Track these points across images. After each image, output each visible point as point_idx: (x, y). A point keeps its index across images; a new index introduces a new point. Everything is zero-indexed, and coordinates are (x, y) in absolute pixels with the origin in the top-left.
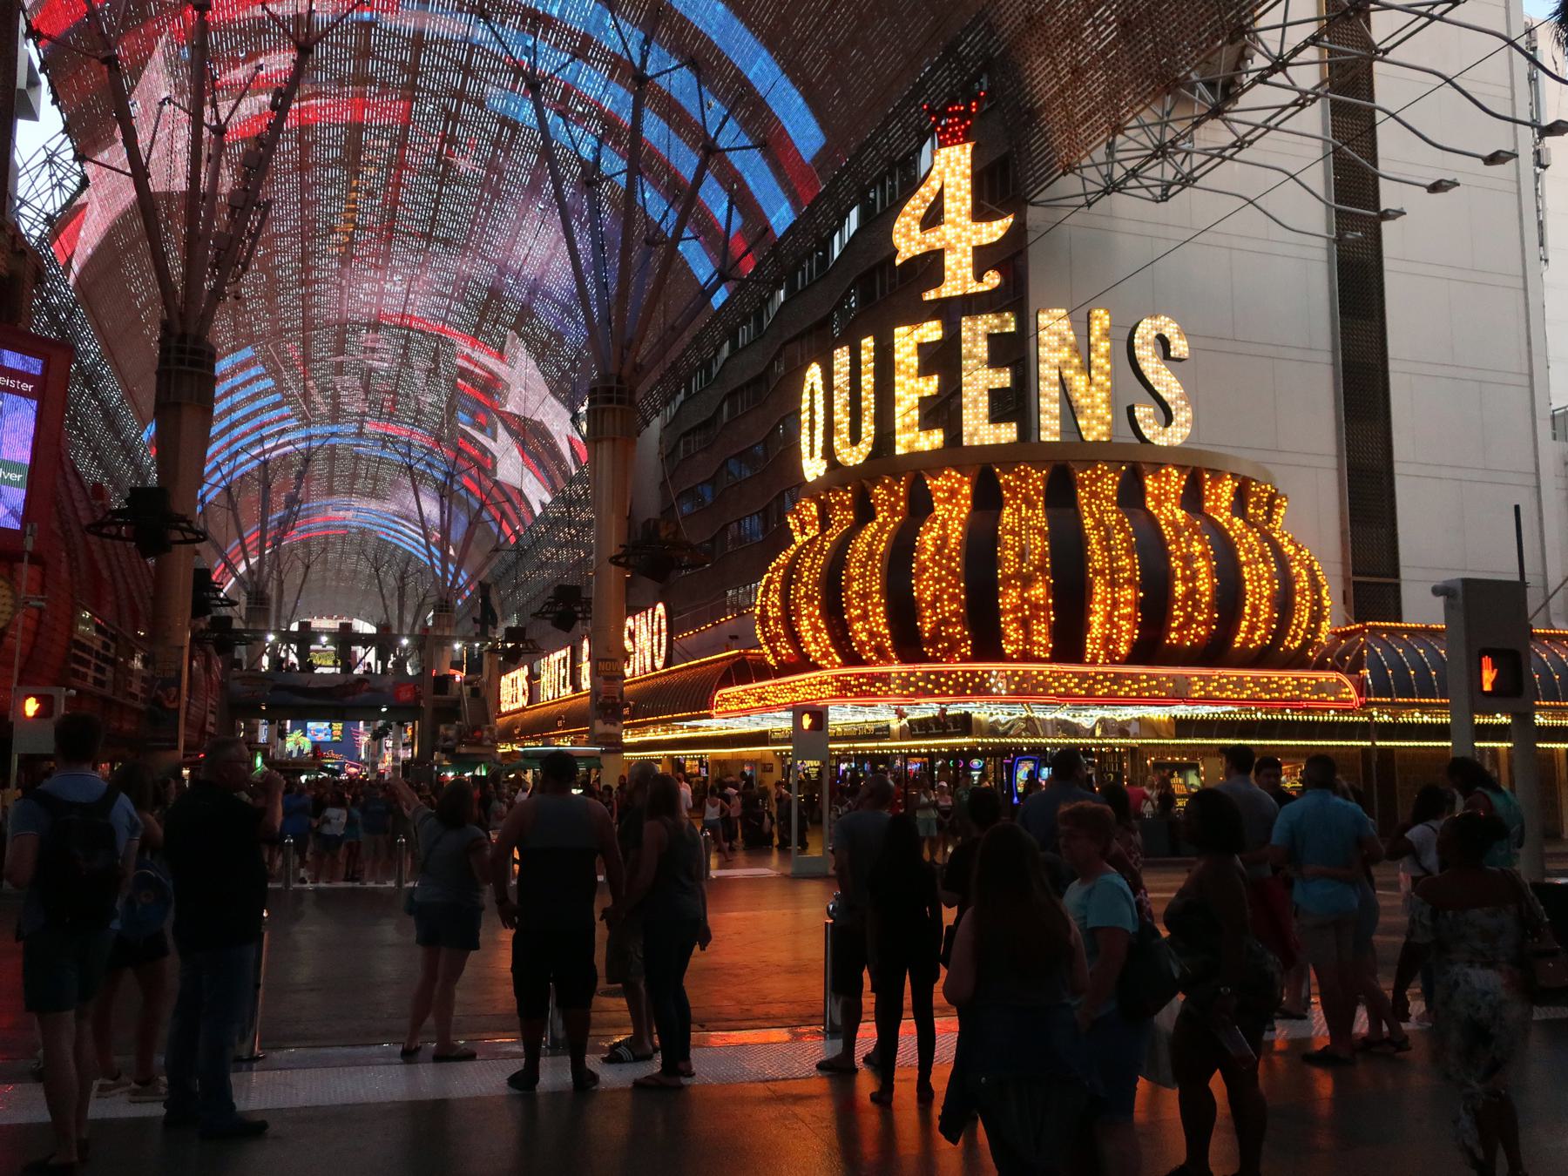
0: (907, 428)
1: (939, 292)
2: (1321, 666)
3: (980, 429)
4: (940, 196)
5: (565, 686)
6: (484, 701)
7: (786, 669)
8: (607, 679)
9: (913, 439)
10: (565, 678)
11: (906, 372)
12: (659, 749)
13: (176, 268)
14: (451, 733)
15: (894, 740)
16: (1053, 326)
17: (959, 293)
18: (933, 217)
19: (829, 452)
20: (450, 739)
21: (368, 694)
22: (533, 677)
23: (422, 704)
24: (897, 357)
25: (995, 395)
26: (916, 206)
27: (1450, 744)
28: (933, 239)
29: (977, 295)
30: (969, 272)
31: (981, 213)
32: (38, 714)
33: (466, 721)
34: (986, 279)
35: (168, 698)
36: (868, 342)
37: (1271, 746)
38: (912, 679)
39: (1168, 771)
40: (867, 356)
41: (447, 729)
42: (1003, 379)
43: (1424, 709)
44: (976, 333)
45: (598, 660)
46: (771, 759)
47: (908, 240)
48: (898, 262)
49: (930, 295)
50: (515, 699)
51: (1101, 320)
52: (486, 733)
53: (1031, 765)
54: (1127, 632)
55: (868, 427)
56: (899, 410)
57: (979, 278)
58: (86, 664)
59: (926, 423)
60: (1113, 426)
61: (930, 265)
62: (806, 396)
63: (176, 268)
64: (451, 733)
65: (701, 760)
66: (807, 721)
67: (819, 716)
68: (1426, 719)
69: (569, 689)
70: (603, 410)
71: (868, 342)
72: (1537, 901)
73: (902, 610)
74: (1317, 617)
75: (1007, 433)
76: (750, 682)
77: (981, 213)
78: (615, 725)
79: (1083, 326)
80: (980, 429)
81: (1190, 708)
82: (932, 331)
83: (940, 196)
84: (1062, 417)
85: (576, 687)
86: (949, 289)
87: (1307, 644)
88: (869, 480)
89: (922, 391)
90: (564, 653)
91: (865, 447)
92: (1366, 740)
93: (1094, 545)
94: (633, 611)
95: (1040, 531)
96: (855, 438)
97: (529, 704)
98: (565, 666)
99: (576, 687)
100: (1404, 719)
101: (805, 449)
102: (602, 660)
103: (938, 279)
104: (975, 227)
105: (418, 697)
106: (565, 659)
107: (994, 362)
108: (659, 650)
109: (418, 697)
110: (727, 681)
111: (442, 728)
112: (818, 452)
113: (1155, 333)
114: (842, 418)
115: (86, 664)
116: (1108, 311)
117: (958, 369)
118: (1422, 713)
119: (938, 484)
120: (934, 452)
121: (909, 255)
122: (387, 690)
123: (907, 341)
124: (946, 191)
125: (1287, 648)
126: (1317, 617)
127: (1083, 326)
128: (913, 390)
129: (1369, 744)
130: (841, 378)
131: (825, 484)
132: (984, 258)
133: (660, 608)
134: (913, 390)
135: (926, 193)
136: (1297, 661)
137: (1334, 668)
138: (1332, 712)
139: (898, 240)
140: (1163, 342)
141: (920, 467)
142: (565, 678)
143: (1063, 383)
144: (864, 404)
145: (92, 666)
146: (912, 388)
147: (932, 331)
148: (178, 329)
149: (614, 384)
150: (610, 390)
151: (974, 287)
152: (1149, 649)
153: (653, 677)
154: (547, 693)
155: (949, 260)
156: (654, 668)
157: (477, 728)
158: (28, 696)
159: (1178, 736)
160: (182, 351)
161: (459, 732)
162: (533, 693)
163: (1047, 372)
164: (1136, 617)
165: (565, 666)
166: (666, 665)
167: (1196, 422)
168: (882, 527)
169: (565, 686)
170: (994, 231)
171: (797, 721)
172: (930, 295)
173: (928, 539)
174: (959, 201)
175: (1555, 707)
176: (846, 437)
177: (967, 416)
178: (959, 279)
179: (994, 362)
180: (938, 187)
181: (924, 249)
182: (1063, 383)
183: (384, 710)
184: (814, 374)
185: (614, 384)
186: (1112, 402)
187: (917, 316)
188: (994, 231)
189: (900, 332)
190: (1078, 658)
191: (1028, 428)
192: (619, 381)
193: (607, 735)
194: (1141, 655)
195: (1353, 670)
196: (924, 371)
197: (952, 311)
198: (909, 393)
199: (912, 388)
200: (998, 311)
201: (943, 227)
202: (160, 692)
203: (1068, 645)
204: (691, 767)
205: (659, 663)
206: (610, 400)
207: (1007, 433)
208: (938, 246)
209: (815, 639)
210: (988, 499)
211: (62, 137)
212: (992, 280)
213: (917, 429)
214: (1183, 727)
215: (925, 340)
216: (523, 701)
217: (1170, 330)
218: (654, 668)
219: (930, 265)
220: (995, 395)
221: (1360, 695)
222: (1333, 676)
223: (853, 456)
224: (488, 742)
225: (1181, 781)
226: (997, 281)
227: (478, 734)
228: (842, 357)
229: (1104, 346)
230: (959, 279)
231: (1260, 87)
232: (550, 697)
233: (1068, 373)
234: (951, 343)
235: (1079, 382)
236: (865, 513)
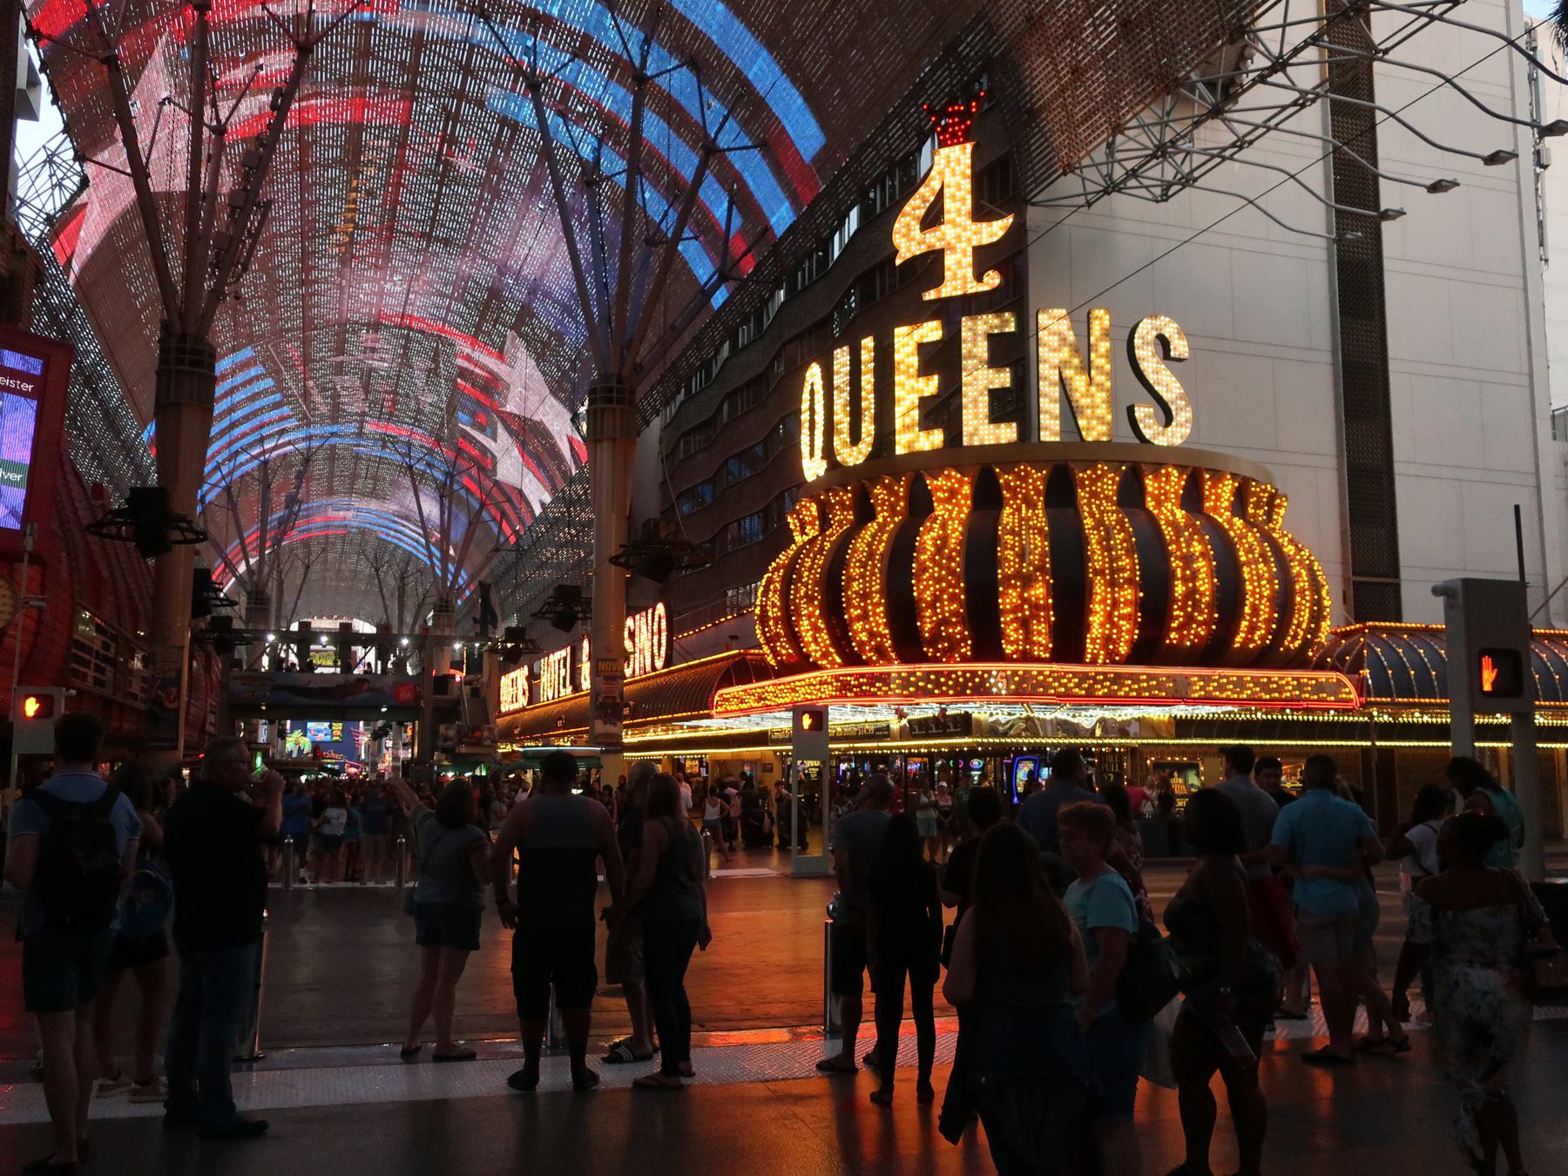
0: (907, 428)
1: (939, 292)
2: (1321, 666)
3: (980, 429)
4: (940, 196)
5: (565, 686)
7: (786, 669)
8: (607, 679)
9: (913, 439)
10: (565, 678)
11: (906, 372)
12: (659, 749)
13: (176, 268)
14: (451, 733)
15: (894, 740)
16: (1053, 326)
17: (959, 293)
18: (933, 217)
19: (829, 452)
20: (450, 739)
21: (368, 694)
23: (422, 704)
24: (897, 357)
25: (995, 395)
26: (916, 206)
27: (1450, 744)
28: (933, 239)
29: (977, 295)
30: (969, 272)
31: (981, 213)
32: (38, 714)
33: (466, 721)
34: (986, 279)
35: (168, 698)
36: (868, 342)
37: (1271, 746)
38: (912, 679)
39: (1168, 771)
40: (867, 356)
41: (447, 729)
42: (1003, 379)
43: (1424, 709)
44: (976, 333)
45: (598, 660)
46: (771, 759)
47: (908, 240)
48: (898, 262)
49: (930, 295)
50: (515, 699)
51: (1101, 320)
52: (486, 733)
53: (1031, 765)
54: (1127, 632)
55: (868, 427)
56: (899, 410)
57: (979, 278)
58: (86, 664)
59: (926, 423)
60: (1113, 426)
61: (930, 265)
62: (806, 396)
63: (176, 268)
64: (451, 733)
65: (701, 760)
66: (807, 721)
67: (819, 716)
68: (1426, 719)
69: (569, 689)
70: (603, 410)
71: (868, 342)
72: (1537, 901)
73: (902, 610)
74: (1317, 617)
75: (1007, 433)
76: (750, 682)
77: (981, 213)
78: (615, 725)
79: (1083, 326)
80: (980, 429)
81: (1190, 708)
82: (932, 331)
83: (940, 196)
84: (1062, 417)
85: (576, 687)
86: (949, 289)
87: (1307, 644)
88: (869, 480)
89: (922, 391)
90: (564, 653)
91: (865, 447)
92: (1366, 740)
93: (1094, 545)
94: (633, 611)
95: (1040, 531)
96: (855, 438)
97: (529, 704)
98: (565, 666)
99: (576, 687)
100: (1404, 719)
101: (805, 449)
102: (602, 660)
103: (938, 279)
104: (975, 227)
105: (418, 697)
106: (565, 659)
107: (994, 362)
108: (659, 650)
109: (418, 697)
110: (727, 681)
111: (442, 728)
112: (818, 452)
113: (1155, 333)
114: (842, 418)
115: (86, 664)
116: (1108, 311)
117: (958, 369)
118: (1422, 713)
119: (938, 484)
120: (934, 452)
121: (909, 255)
122: (387, 690)
123: (907, 341)
124: (946, 191)
125: (1287, 648)
126: (1317, 617)
127: (1083, 326)
128: (913, 390)
129: (1369, 744)
130: (841, 378)
131: (825, 484)
132: (984, 258)
133: (660, 608)
134: (913, 390)
135: (926, 193)
136: (1297, 661)
137: (1334, 668)
138: (1332, 712)
139: (898, 240)
140: (1163, 342)
141: (920, 467)
142: (565, 678)
143: (1063, 383)
144: (864, 404)
145: (92, 666)
146: (912, 388)
147: (932, 331)
148: (178, 329)
149: (614, 384)
150: (610, 390)
151: (974, 287)
152: (1149, 649)
153: (653, 677)
154: (547, 693)
155: (949, 260)
156: (654, 668)
157: (477, 728)
158: (28, 696)
159: (1178, 736)
161: (459, 732)
162: (533, 693)
163: (1047, 372)
164: (1136, 617)
165: (565, 666)
166: (666, 665)
167: (1196, 422)
168: (882, 527)
169: (565, 686)
170: (994, 231)
171: (797, 721)
172: (930, 295)
173: (928, 539)
174: (959, 201)
176: (846, 437)
178: (959, 279)
179: (994, 362)
180: (938, 187)
181: (924, 249)
182: (1063, 383)
183: (384, 710)
184: (814, 374)
185: (614, 384)
186: (1112, 402)
187: (917, 316)
188: (994, 231)
189: (900, 332)
190: (1078, 658)
191: (1028, 428)
192: (619, 381)
193: (607, 735)
195: (1353, 670)
196: (924, 371)
197: (952, 311)
198: (909, 393)
199: (912, 388)
200: (998, 311)
201: (943, 227)
202: (160, 692)
203: (1068, 645)
204: (691, 767)
205: (659, 663)
206: (610, 400)
207: (1007, 433)
208: (938, 246)
209: (815, 639)
210: (988, 499)
212: (992, 280)
213: (917, 429)
214: (1183, 727)
215: (925, 340)
216: (523, 701)
217: (1170, 330)
218: (654, 668)
219: (930, 265)
220: (995, 395)
221: (1360, 695)
222: (1333, 676)
223: (853, 456)
224: (488, 742)
225: (1181, 781)
226: (997, 281)
227: (478, 734)
228: (842, 357)
229: (1104, 346)
230: (959, 279)
232: (550, 697)
233: (1068, 373)
234: (951, 343)
235: (1079, 382)
236: (865, 513)
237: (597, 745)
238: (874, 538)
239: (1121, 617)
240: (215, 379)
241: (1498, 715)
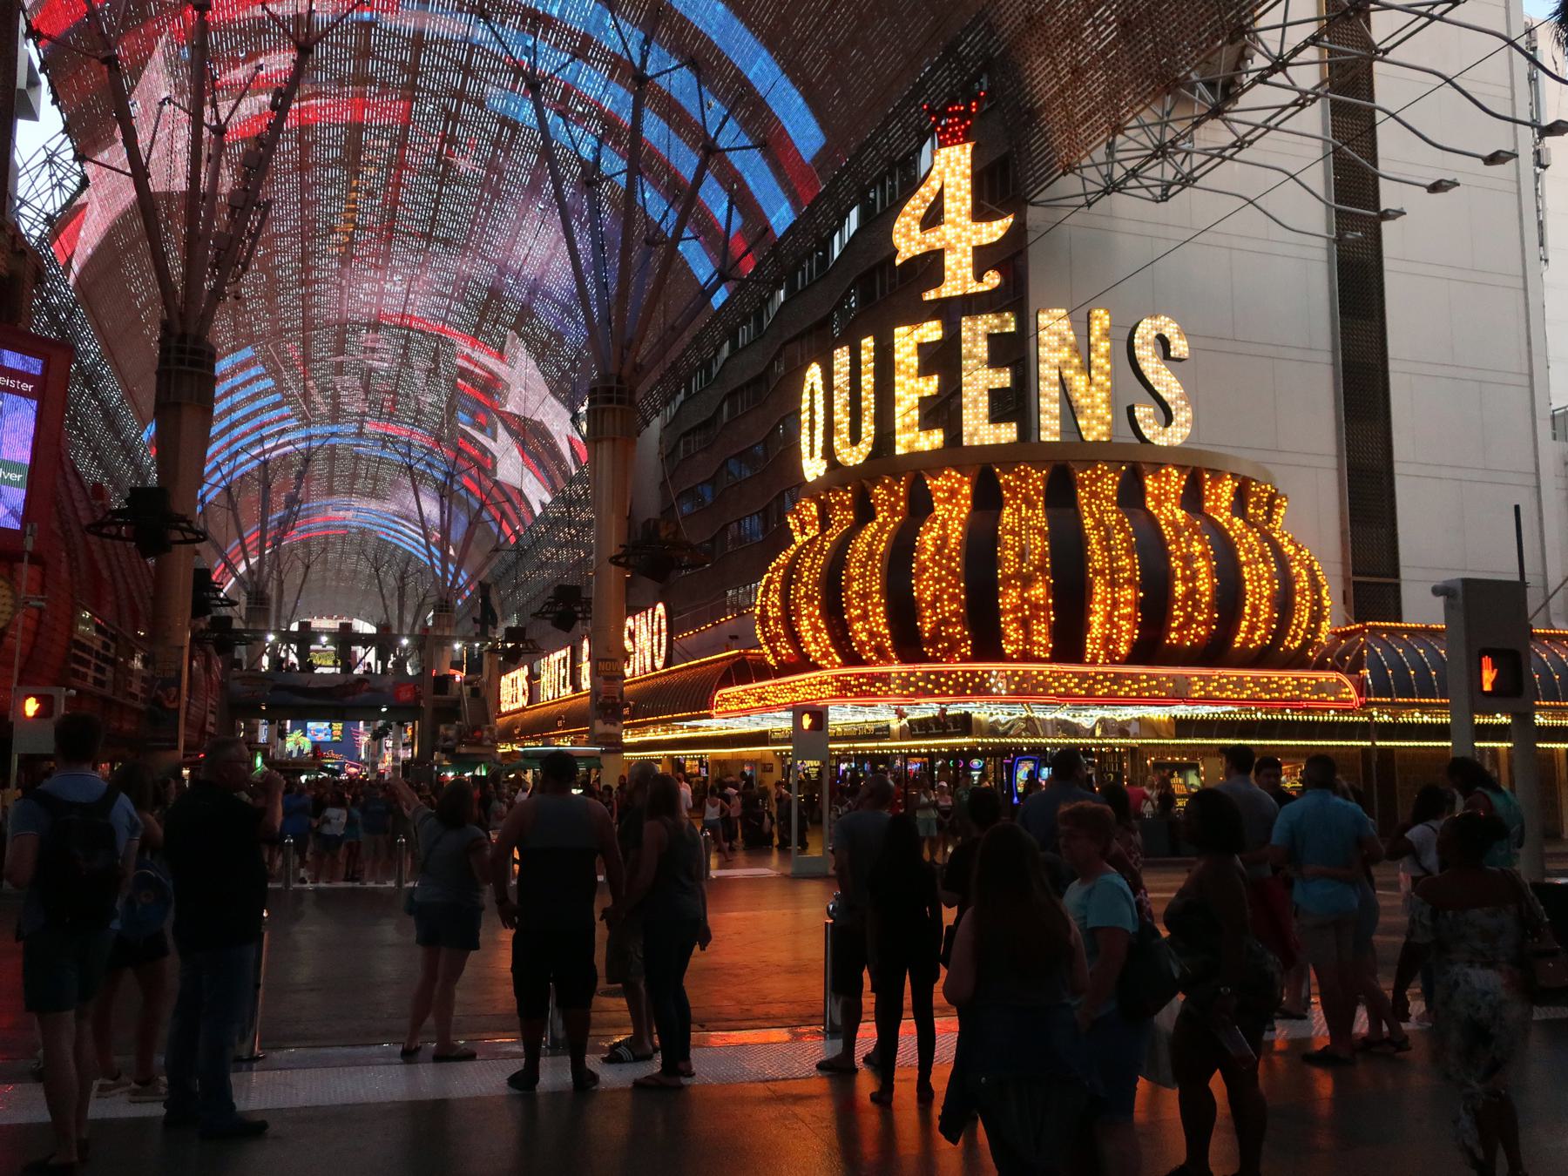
0: (907, 428)
1: (939, 292)
2: (1321, 666)
3: (980, 429)
4: (940, 196)
5: (565, 686)
6: (484, 701)
7: (786, 669)
8: (607, 679)
9: (913, 439)
10: (565, 678)
11: (906, 372)
12: (659, 749)
13: (176, 268)
14: (451, 733)
15: (894, 740)
16: (1053, 326)
17: (959, 293)
18: (933, 217)
19: (829, 452)
20: (450, 739)
21: (368, 694)
22: (533, 677)
23: (422, 704)
24: (897, 357)
25: (995, 395)
26: (916, 206)
27: (1450, 744)
28: (933, 239)
29: (977, 295)
30: (969, 272)
31: (981, 213)
32: (38, 714)
33: (466, 721)
34: (986, 279)
35: (168, 698)
36: (868, 342)
37: (1271, 746)
38: (912, 679)
39: (1168, 771)
40: (867, 356)
41: (447, 729)
42: (1003, 379)
43: (1424, 709)
44: (976, 333)
45: (598, 660)
46: (771, 759)
47: (908, 240)
48: (898, 262)
49: (930, 295)
50: (515, 699)
51: (1101, 320)
52: (486, 733)
54: (1127, 632)
55: (868, 427)
56: (899, 410)
57: (979, 278)
58: (86, 664)
59: (926, 423)
61: (930, 265)
62: (806, 396)
63: (176, 268)
64: (451, 733)
65: (701, 760)
66: (807, 721)
67: (819, 716)
68: (1426, 719)
69: (569, 689)
70: (603, 410)
71: (868, 342)
72: (1537, 901)
73: (902, 610)
74: (1317, 617)
75: (1007, 433)
76: (750, 682)
77: (981, 213)
78: (615, 725)
79: (1083, 326)
80: (980, 429)
81: (1190, 708)
82: (932, 331)
83: (940, 196)
84: (1062, 417)
85: (576, 687)
86: (949, 289)
87: (1307, 644)
88: (869, 480)
89: (922, 391)
90: (564, 653)
91: (865, 447)
92: (1366, 740)
93: (1094, 545)
94: (633, 611)
95: (1040, 531)
96: (855, 438)
97: (529, 704)
98: (565, 666)
99: (576, 687)
100: (1404, 719)
101: (805, 449)
102: (602, 660)
103: (938, 279)
104: (975, 227)
105: (418, 697)
106: (565, 659)
107: (994, 362)
108: (659, 650)
109: (418, 697)
110: (727, 681)
111: (442, 728)
113: (1155, 333)
114: (842, 418)
115: (86, 664)
116: (1108, 311)
117: (958, 369)
118: (1422, 713)
119: (938, 484)
120: (934, 452)
121: (909, 255)
122: (387, 690)
123: (907, 341)
124: (946, 191)
125: (1287, 648)
126: (1317, 617)
127: (1083, 326)
128: (913, 390)
129: (1369, 744)
130: (841, 378)
131: (825, 484)
132: (984, 258)
133: (660, 608)
134: (913, 390)
135: (926, 193)
136: (1297, 661)
137: (1334, 668)
138: (1332, 712)
139: (898, 240)
140: (1163, 342)
141: (920, 467)
142: (565, 678)
143: (1063, 383)
145: (92, 666)
146: (912, 388)
147: (932, 331)
148: (178, 329)
149: (614, 384)
150: (610, 390)
151: (974, 287)
152: (1149, 649)
153: (653, 677)
154: (547, 693)
155: (949, 260)
156: (654, 668)
157: (477, 728)
158: (28, 696)
159: (1178, 736)
160: (182, 351)
161: (459, 732)
162: (533, 693)
163: (1047, 372)
164: (1136, 617)
165: (565, 666)
166: (666, 665)
168: (882, 527)
169: (565, 686)
170: (994, 231)
171: (797, 721)
172: (930, 295)
173: (928, 539)
174: (959, 201)
175: (1555, 707)
176: (846, 437)
177: (967, 416)
178: (959, 279)
179: (994, 362)
180: (938, 187)
181: (924, 249)
182: (1063, 383)
183: (384, 710)
184: (814, 374)
185: (614, 384)
186: (1112, 402)
187: (917, 316)
188: (994, 231)
189: (900, 332)
190: (1078, 658)
191: (1028, 428)
192: (619, 381)
193: (607, 735)
194: (1141, 655)
195: (1353, 670)
196: (924, 371)
197: (952, 311)
198: (909, 393)
199: (912, 388)
200: (998, 311)
201: (943, 227)
202: (160, 692)
203: (1068, 645)
204: (691, 767)
205: (659, 663)
206: (610, 400)
207: (1007, 433)
208: (938, 246)
209: (815, 639)
210: (988, 499)
211: (62, 137)
212: (992, 280)
213: (917, 429)
214: (1183, 727)
215: (925, 340)
216: (523, 701)
217: (1170, 330)
218: (654, 668)
219: (930, 265)
220: (995, 395)
221: (1360, 695)
222: (1333, 676)
223: (853, 456)
224: (488, 742)
225: (1181, 781)
226: (997, 281)
227: (478, 734)
228: (842, 357)
229: (1104, 346)
230: (959, 279)
231: (1260, 87)
232: (550, 697)
233: (1068, 373)
234: (951, 343)
235: (1079, 382)
236: (865, 513)
237: (597, 745)
238: (874, 538)
239: (1121, 617)
240: (215, 379)
241: (1498, 715)
